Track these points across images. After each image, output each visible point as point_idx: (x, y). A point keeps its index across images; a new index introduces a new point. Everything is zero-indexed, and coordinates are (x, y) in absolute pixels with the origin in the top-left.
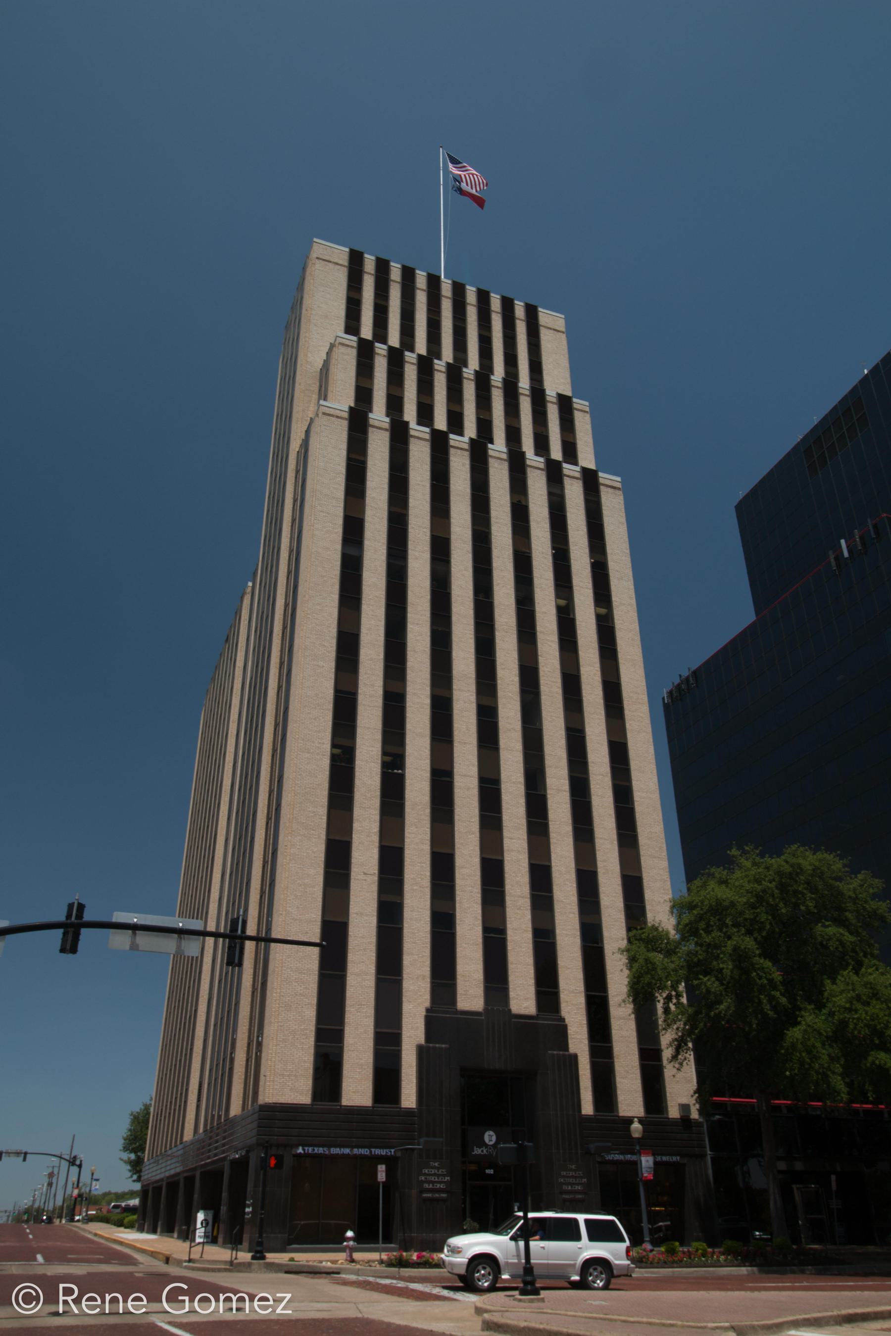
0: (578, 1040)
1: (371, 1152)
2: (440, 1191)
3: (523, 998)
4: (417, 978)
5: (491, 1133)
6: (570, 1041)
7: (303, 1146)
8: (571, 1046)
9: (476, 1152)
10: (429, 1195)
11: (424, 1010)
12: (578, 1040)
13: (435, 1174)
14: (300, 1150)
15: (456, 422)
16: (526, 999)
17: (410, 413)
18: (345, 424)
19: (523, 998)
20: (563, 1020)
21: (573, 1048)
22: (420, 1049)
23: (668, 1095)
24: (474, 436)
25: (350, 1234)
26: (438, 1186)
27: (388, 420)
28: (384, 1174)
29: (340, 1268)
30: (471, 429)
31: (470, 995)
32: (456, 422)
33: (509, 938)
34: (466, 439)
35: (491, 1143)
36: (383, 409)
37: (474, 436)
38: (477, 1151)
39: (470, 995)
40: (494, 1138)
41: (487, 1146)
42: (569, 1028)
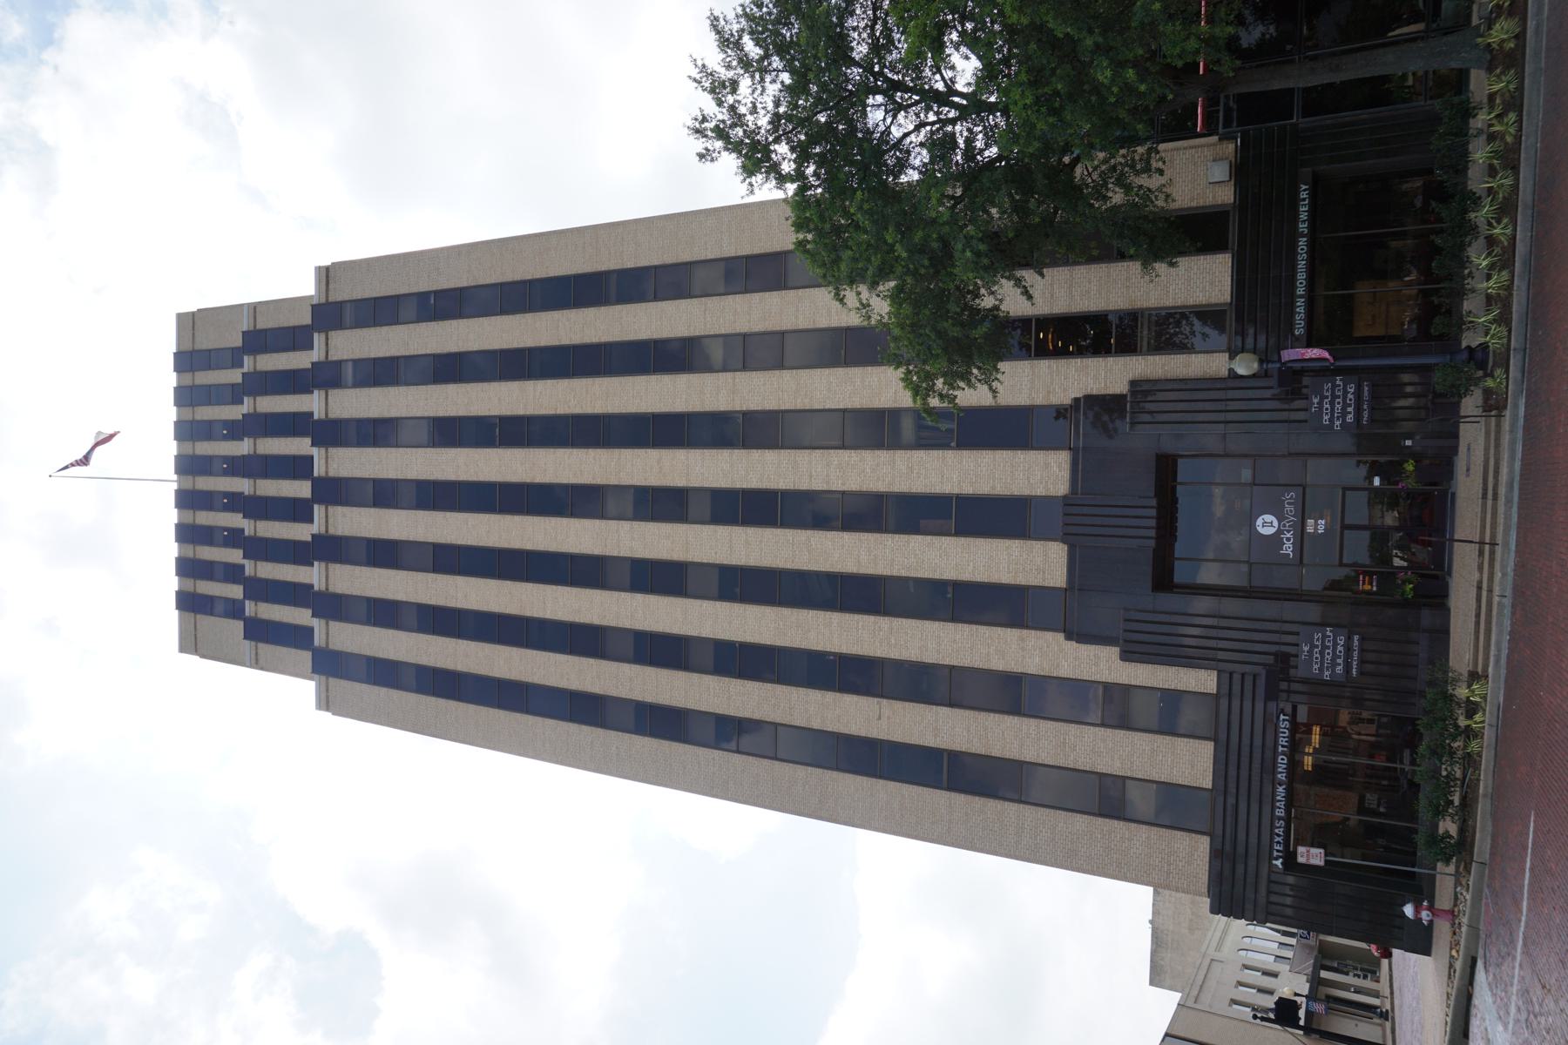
0: (1107, 375)
1: (1283, 753)
2: (1348, 649)
3: (1042, 473)
4: (1023, 649)
5: (1259, 522)
6: (1111, 391)
7: (1271, 858)
8: (1118, 391)
9: (1289, 551)
10: (1366, 415)
11: (1069, 643)
12: (1107, 375)
13: (1322, 653)
14: (1279, 863)
15: (298, 467)
16: (1047, 465)
17: (300, 532)
18: (333, 451)
19: (1042, 473)
20: (1077, 400)
21: (1119, 387)
22: (1126, 656)
23: (1194, 204)
24: (308, 441)
25: (1409, 910)
26: (1340, 648)
27: (316, 392)
28: (1314, 851)
29: (1465, 955)
30: (299, 446)
31: (1040, 563)
32: (298, 467)
33: (956, 491)
34: (315, 451)
35: (1276, 523)
36: (305, 398)
37: (308, 441)
38: (1288, 548)
39: (1040, 563)
40: (1269, 518)
41: (1279, 532)
42: (1089, 392)
